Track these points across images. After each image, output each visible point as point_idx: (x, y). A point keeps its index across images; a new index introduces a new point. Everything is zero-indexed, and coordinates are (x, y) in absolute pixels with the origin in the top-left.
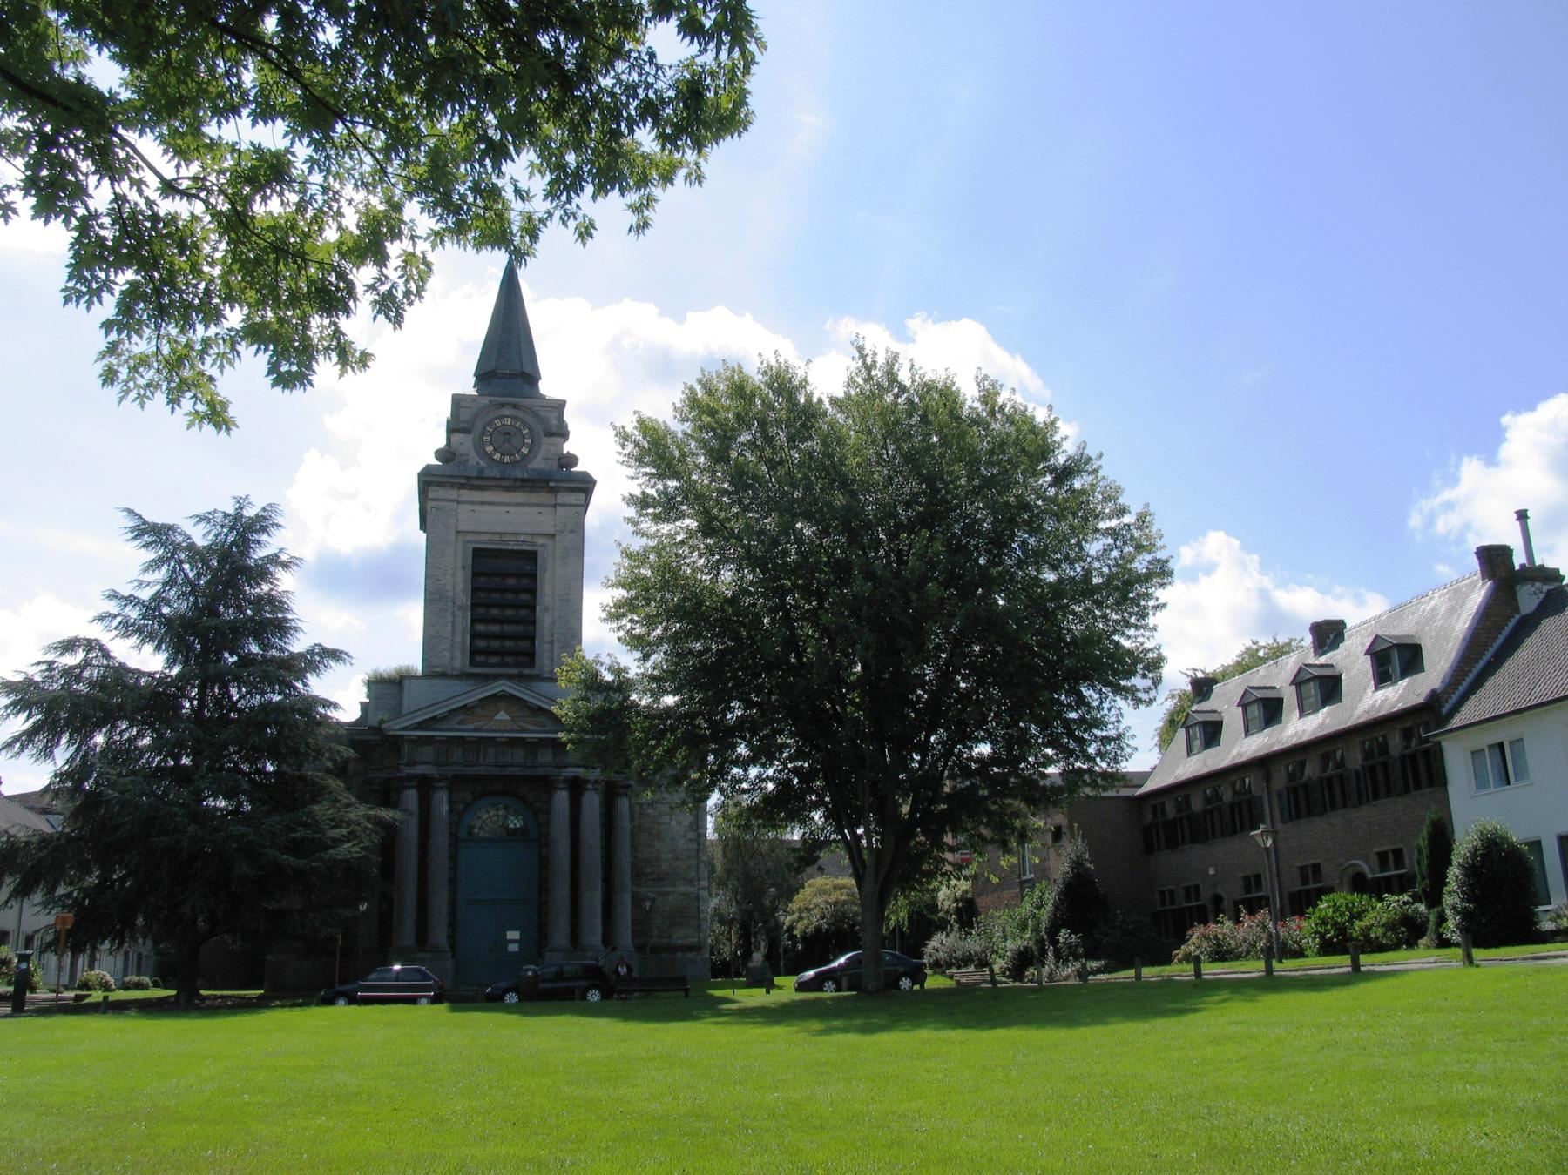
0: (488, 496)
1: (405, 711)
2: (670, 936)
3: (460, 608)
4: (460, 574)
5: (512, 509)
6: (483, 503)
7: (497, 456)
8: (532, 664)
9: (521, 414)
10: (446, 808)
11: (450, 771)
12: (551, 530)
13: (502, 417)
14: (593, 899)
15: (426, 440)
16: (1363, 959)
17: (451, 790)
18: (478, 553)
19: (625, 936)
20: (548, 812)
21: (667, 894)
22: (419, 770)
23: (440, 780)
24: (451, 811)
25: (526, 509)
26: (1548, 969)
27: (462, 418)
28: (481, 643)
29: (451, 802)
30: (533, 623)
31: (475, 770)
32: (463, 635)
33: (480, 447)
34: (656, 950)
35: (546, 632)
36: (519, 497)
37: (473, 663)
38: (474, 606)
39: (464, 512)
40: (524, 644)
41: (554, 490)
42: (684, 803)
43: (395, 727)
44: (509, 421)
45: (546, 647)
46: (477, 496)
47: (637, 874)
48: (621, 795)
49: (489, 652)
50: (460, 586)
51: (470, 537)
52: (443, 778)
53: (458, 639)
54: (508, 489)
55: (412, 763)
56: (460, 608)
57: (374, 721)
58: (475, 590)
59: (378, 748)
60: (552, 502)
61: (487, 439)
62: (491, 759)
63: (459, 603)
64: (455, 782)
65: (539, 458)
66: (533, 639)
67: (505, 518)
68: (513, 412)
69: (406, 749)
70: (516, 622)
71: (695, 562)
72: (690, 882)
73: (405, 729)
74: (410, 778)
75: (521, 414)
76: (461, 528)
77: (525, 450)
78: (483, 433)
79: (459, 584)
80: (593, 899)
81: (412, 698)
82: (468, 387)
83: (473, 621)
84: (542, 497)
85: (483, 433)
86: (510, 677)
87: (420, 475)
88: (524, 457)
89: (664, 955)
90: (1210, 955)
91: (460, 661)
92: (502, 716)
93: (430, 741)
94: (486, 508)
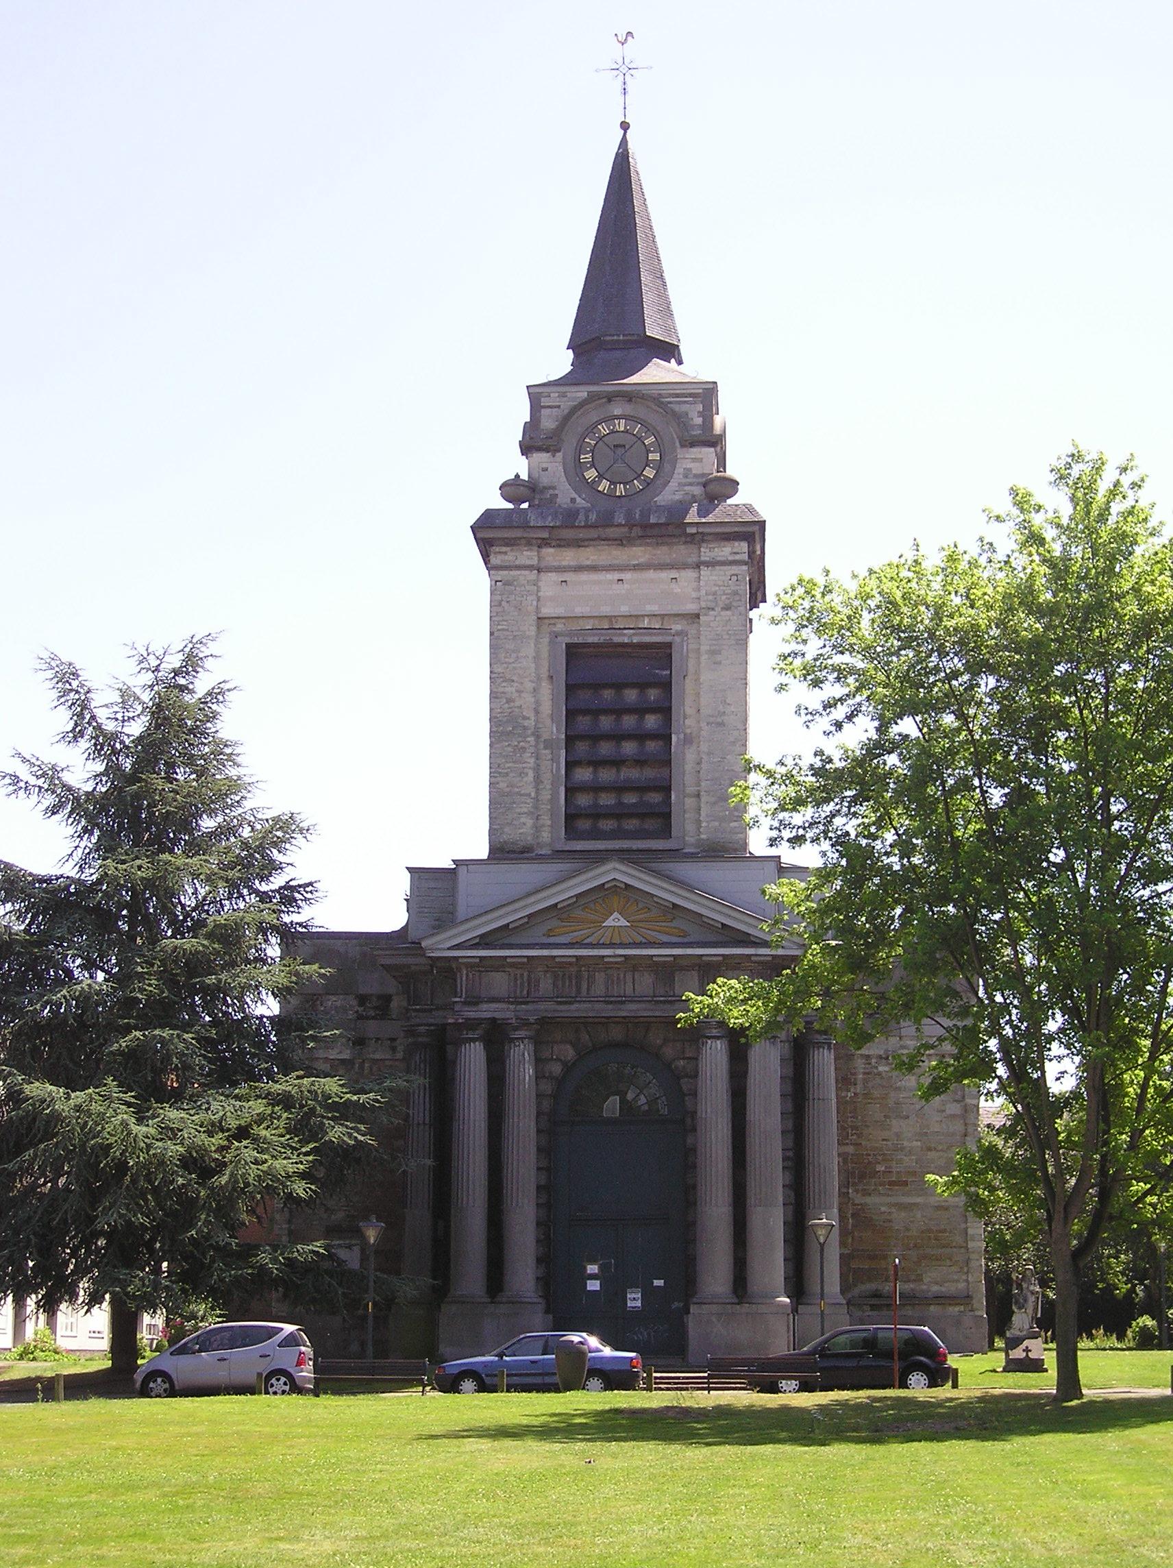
0: (589, 556)
1: (461, 912)
2: (919, 1279)
3: (548, 744)
4: (546, 690)
5: (627, 576)
6: (579, 569)
7: (604, 486)
8: (666, 832)
9: (654, 419)
11: (532, 1011)
12: (691, 607)
14: (770, 1223)
15: (492, 461)
17: (538, 1043)
18: (574, 652)
19: (829, 1275)
20: (695, 1075)
21: (909, 1207)
22: (487, 1011)
23: (516, 1029)
24: (539, 1076)
25: (651, 574)
27: (548, 427)
28: (583, 800)
29: (538, 1061)
30: (668, 763)
31: (575, 1010)
32: (554, 784)
33: (575, 470)
35: (689, 779)
36: (639, 553)
37: (571, 831)
38: (570, 740)
39: (549, 583)
40: (655, 798)
43: (441, 945)
44: (621, 425)
45: (690, 802)
46: (568, 557)
47: (858, 1172)
48: (819, 1045)
49: (596, 814)
50: (546, 708)
51: (560, 627)
53: (546, 795)
54: (621, 542)
55: (473, 1001)
56: (548, 744)
57: (413, 935)
58: (571, 714)
59: (394, 992)
60: (693, 559)
61: (586, 458)
62: (599, 989)
63: (546, 736)
65: (673, 484)
66: (667, 790)
67: (615, 592)
68: (628, 409)
69: (463, 978)
70: (640, 763)
71: (1040, 582)
73: (457, 947)
74: (471, 1024)
76: (546, 611)
77: (649, 473)
78: (580, 450)
79: (544, 704)
80: (770, 1223)
81: (469, 896)
82: (561, 363)
83: (570, 766)
84: (681, 552)
85: (580, 450)
86: (626, 856)
87: (474, 528)
88: (648, 483)
91: (550, 833)
92: (616, 920)
93: (500, 965)
94: (584, 577)
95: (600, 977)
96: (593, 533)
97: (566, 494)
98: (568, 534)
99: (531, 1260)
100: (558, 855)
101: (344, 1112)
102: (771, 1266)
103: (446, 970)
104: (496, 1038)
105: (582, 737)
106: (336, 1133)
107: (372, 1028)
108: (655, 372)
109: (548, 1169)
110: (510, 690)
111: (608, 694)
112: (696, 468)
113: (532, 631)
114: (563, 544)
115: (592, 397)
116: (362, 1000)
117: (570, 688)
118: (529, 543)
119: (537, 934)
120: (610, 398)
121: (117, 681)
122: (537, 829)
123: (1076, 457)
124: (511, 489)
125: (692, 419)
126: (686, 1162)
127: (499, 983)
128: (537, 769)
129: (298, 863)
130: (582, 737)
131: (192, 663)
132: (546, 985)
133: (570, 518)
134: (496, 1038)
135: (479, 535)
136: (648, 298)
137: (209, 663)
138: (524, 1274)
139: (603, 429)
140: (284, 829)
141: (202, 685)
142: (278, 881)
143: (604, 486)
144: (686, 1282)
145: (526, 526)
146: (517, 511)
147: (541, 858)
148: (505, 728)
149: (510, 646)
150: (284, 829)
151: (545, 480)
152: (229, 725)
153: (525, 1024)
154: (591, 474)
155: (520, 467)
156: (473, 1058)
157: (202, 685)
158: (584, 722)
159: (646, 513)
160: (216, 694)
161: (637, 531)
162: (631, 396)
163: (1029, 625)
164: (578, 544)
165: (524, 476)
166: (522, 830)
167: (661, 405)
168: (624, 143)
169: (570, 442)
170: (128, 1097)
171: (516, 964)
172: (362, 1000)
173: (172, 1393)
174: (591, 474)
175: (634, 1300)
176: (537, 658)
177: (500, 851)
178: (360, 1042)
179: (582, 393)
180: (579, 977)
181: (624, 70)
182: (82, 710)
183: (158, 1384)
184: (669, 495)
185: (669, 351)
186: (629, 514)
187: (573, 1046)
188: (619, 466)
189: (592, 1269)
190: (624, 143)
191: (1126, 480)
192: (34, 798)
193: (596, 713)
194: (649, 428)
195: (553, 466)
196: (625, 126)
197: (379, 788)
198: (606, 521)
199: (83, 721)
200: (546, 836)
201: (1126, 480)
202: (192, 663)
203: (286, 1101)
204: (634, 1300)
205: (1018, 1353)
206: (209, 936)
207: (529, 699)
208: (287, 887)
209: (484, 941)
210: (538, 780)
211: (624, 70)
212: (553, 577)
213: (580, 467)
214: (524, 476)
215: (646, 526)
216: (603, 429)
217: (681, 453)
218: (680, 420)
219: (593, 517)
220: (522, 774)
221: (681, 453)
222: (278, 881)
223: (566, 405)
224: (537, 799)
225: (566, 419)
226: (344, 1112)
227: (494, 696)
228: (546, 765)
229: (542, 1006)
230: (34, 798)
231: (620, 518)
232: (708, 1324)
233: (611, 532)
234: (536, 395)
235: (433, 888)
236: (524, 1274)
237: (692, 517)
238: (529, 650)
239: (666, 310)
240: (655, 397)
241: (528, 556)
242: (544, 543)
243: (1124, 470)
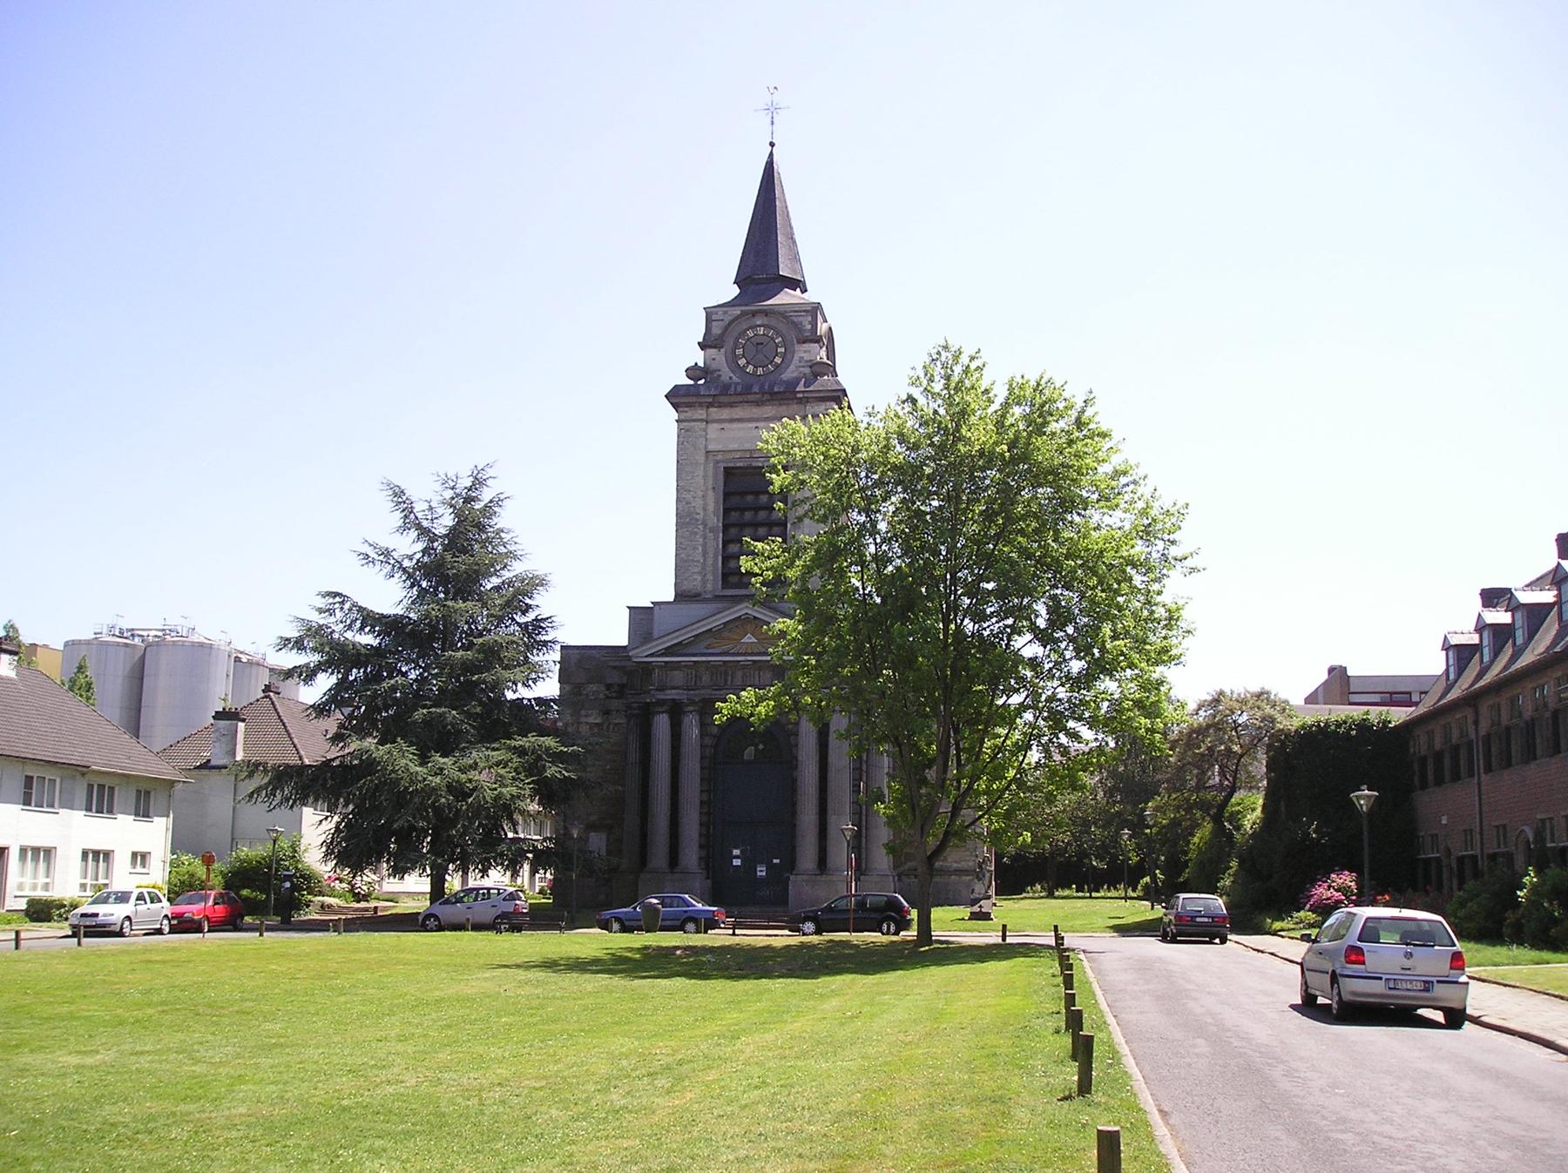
0: (738, 412)
6: (732, 421)
7: (750, 369)
9: (781, 326)
15: (682, 353)
18: (729, 472)
22: (671, 694)
24: (702, 735)
27: (720, 330)
32: (716, 557)
33: (732, 360)
37: (726, 583)
38: (726, 527)
43: (641, 655)
44: (761, 331)
46: (725, 413)
50: (711, 507)
51: (720, 457)
53: (710, 561)
54: (758, 403)
55: (662, 689)
58: (726, 511)
61: (739, 352)
65: (792, 367)
68: (765, 321)
74: (664, 702)
76: (710, 448)
77: (778, 360)
79: (710, 506)
81: (660, 624)
83: (725, 543)
88: (777, 366)
92: (749, 639)
94: (735, 425)
95: (739, 674)
96: (740, 398)
97: (726, 374)
98: (723, 399)
99: (695, 847)
100: (717, 598)
101: (558, 758)
102: (840, 854)
103: (646, 669)
104: (676, 711)
105: (734, 525)
106: (551, 771)
107: (615, 704)
108: (786, 297)
109: (709, 791)
110: (688, 496)
111: (750, 498)
112: (807, 357)
113: (702, 459)
114: (721, 405)
115: (743, 314)
116: (609, 687)
117: (727, 495)
118: (701, 405)
119: (701, 648)
120: (754, 314)
121: (427, 494)
122: (704, 582)
123: (946, 348)
124: (692, 372)
125: (807, 326)
126: (791, 788)
127: (678, 677)
128: (704, 545)
129: (543, 604)
130: (734, 525)
131: (478, 482)
132: (706, 678)
133: (725, 389)
134: (676, 711)
135: (675, 400)
136: (782, 252)
137: (489, 482)
138: (691, 855)
139: (750, 333)
140: (533, 583)
141: (486, 495)
142: (531, 616)
143: (750, 369)
144: (791, 863)
145: (698, 395)
146: (695, 385)
147: (706, 600)
148: (685, 520)
149: (688, 469)
150: (533, 583)
151: (714, 366)
152: (503, 520)
153: (693, 703)
154: (742, 362)
155: (699, 358)
156: (662, 723)
157: (486, 495)
158: (735, 515)
159: (772, 386)
160: (497, 501)
161: (767, 397)
162: (766, 313)
163: (899, 453)
164: (731, 405)
165: (701, 364)
166: (695, 583)
167: (786, 318)
168: (771, 154)
169: (730, 342)
170: (412, 749)
171: (688, 666)
172: (609, 687)
173: (440, 928)
174: (742, 362)
175: (761, 871)
176: (705, 477)
177: (682, 596)
178: (607, 713)
179: (737, 311)
180: (726, 673)
181: (772, 111)
182: (408, 511)
183: (432, 923)
184: (789, 374)
185: (797, 284)
186: (762, 386)
188: (760, 356)
189: (736, 852)
190: (771, 154)
191: (973, 366)
192: (378, 567)
193: (743, 510)
194: (778, 334)
195: (719, 356)
196: (772, 144)
197: (601, 559)
198: (747, 390)
199: (410, 521)
200: (709, 586)
201: (973, 366)
202: (478, 482)
203: (521, 752)
204: (761, 871)
205: (976, 909)
206: (479, 652)
207: (699, 503)
208: (536, 620)
209: (668, 651)
210: (705, 553)
211: (772, 111)
212: (715, 425)
213: (736, 358)
214: (701, 364)
215: (773, 394)
216: (750, 333)
217: (797, 347)
218: (797, 326)
219: (739, 389)
220: (695, 548)
221: (797, 347)
222: (531, 616)
223: (728, 319)
224: (704, 564)
225: (726, 329)
226: (558, 758)
227: (678, 500)
228: (711, 543)
230: (378, 567)
231: (756, 389)
232: (804, 888)
233: (751, 397)
234: (710, 313)
235: (641, 618)
236: (691, 855)
237: (800, 388)
238: (701, 472)
239: (795, 258)
240: (783, 314)
241: (700, 413)
242: (710, 405)
243: (972, 359)
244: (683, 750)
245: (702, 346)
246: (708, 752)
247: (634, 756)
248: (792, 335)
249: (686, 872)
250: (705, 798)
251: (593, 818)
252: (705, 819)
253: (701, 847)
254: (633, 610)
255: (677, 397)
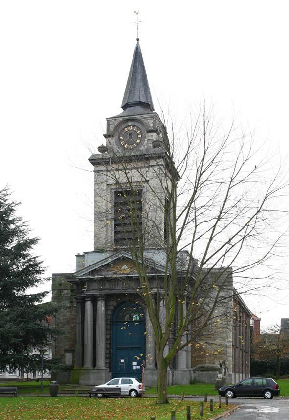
9: (140, 125)
10: (103, 308)
11: (103, 293)
13: (128, 126)
16: (41, 378)
22: (91, 293)
23: (99, 297)
26: (281, 402)
29: (106, 306)
34: (203, 369)
41: (147, 159)
42: (55, 316)
44: (131, 128)
52: (101, 296)
61: (122, 138)
64: (108, 298)
68: (133, 123)
72: (224, 339)
75: (136, 124)
77: (138, 141)
88: (138, 144)
89: (211, 372)
90: (225, 379)
92: (125, 267)
104: (94, 300)
109: (110, 330)
124: (102, 149)
138: (101, 362)
139: (126, 129)
143: (126, 146)
148: (99, 216)
155: (104, 142)
156: (89, 305)
168: (138, 44)
178: (72, 302)
187: (116, 302)
190: (138, 44)
196: (138, 40)
214: (105, 145)
223: (116, 123)
229: (106, 291)
234: (109, 121)
236: (101, 362)
241: (103, 168)
244: (98, 314)
245: (105, 136)
246: (109, 317)
247: (79, 320)
248: (144, 129)
249: (99, 369)
250: (108, 337)
251: (67, 347)
252: (108, 337)
253: (106, 358)
254: (282, 319)
255: (94, 161)
